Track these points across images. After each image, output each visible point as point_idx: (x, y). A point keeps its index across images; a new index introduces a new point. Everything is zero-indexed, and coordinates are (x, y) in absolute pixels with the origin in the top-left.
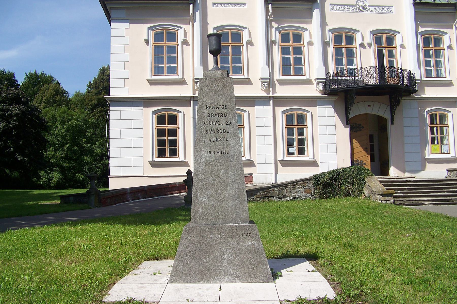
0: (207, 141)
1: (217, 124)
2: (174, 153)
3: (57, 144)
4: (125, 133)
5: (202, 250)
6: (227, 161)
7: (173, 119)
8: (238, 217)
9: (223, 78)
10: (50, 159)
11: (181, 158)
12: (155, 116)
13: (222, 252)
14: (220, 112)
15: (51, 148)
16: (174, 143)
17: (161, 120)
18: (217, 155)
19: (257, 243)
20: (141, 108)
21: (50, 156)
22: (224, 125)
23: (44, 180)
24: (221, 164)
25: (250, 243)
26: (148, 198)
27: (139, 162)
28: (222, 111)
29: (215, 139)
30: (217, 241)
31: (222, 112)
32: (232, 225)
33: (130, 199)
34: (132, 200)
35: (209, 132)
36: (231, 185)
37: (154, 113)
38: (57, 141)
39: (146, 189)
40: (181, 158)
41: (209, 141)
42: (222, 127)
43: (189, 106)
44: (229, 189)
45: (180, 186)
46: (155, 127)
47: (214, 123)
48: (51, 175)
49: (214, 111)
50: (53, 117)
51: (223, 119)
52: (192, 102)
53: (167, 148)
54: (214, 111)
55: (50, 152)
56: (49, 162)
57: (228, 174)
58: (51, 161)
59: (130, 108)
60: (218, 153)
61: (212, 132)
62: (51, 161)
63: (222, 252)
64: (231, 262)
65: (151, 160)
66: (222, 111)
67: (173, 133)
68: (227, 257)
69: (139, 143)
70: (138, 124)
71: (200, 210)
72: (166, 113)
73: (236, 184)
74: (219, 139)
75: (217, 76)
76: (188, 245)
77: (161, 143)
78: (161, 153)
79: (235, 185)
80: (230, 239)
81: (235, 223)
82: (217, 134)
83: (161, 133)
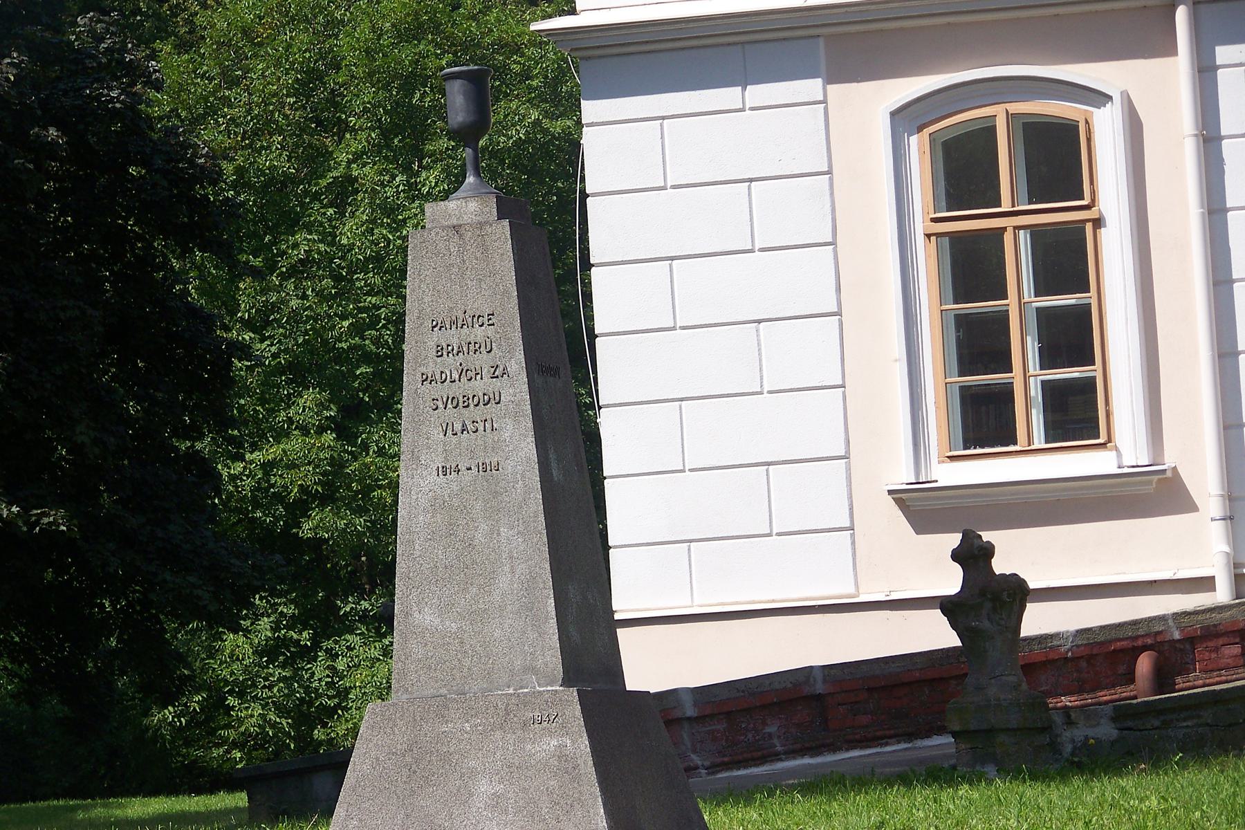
0: (437, 434)
1: (464, 379)
2: (1075, 415)
3: (367, 358)
4: (702, 289)
5: (415, 772)
6: (496, 494)
7: (1057, 159)
8: (533, 670)
9: (481, 225)
10: (299, 509)
11: (1124, 448)
12: (917, 145)
13: (473, 773)
14: (472, 339)
15: (309, 397)
16: (1071, 337)
17: (964, 171)
18: (467, 477)
19: (573, 742)
20: (811, 87)
21: (292, 482)
22: (485, 379)
23: (252, 725)
24: (479, 505)
25: (554, 742)
26: (834, 748)
27: (815, 496)
28: (479, 333)
29: (458, 427)
30: (460, 741)
31: (478, 339)
32: (511, 691)
33: (696, 759)
34: (714, 768)
35: (441, 406)
36: (507, 569)
37: (907, 118)
38: (358, 329)
39: (820, 688)
40: (1124, 448)
41: (441, 435)
42: (479, 386)
43: (1170, 49)
44: (503, 582)
45: (1090, 658)
46: (920, 225)
47: (456, 376)
48: (319, 670)
49: (453, 337)
50: (310, 79)
51: (482, 361)
52: (1181, 15)
53: (1028, 375)
54: (453, 337)
55: (295, 445)
56: (290, 543)
57: (499, 534)
58: (306, 529)
59: (727, 96)
60: (470, 469)
61: (449, 406)
62: (306, 529)
63: (473, 773)
64: (496, 802)
65: (902, 476)
66: (479, 333)
67: (1066, 260)
68: (485, 788)
69: (807, 352)
70: (794, 211)
71: (417, 650)
72: (999, 113)
73: (523, 566)
74: (470, 427)
75: (466, 219)
76: (377, 759)
77: (979, 345)
78: (986, 421)
79: (521, 568)
80: (498, 734)
81: (521, 688)
82: (465, 411)
83: (972, 267)
